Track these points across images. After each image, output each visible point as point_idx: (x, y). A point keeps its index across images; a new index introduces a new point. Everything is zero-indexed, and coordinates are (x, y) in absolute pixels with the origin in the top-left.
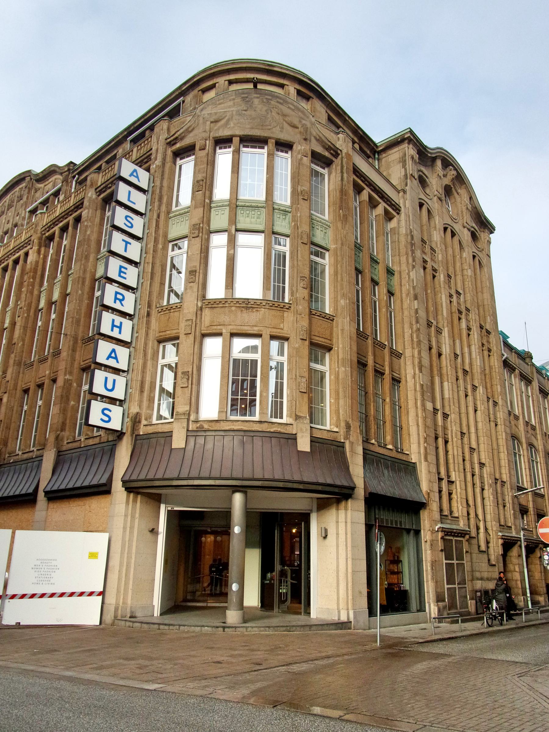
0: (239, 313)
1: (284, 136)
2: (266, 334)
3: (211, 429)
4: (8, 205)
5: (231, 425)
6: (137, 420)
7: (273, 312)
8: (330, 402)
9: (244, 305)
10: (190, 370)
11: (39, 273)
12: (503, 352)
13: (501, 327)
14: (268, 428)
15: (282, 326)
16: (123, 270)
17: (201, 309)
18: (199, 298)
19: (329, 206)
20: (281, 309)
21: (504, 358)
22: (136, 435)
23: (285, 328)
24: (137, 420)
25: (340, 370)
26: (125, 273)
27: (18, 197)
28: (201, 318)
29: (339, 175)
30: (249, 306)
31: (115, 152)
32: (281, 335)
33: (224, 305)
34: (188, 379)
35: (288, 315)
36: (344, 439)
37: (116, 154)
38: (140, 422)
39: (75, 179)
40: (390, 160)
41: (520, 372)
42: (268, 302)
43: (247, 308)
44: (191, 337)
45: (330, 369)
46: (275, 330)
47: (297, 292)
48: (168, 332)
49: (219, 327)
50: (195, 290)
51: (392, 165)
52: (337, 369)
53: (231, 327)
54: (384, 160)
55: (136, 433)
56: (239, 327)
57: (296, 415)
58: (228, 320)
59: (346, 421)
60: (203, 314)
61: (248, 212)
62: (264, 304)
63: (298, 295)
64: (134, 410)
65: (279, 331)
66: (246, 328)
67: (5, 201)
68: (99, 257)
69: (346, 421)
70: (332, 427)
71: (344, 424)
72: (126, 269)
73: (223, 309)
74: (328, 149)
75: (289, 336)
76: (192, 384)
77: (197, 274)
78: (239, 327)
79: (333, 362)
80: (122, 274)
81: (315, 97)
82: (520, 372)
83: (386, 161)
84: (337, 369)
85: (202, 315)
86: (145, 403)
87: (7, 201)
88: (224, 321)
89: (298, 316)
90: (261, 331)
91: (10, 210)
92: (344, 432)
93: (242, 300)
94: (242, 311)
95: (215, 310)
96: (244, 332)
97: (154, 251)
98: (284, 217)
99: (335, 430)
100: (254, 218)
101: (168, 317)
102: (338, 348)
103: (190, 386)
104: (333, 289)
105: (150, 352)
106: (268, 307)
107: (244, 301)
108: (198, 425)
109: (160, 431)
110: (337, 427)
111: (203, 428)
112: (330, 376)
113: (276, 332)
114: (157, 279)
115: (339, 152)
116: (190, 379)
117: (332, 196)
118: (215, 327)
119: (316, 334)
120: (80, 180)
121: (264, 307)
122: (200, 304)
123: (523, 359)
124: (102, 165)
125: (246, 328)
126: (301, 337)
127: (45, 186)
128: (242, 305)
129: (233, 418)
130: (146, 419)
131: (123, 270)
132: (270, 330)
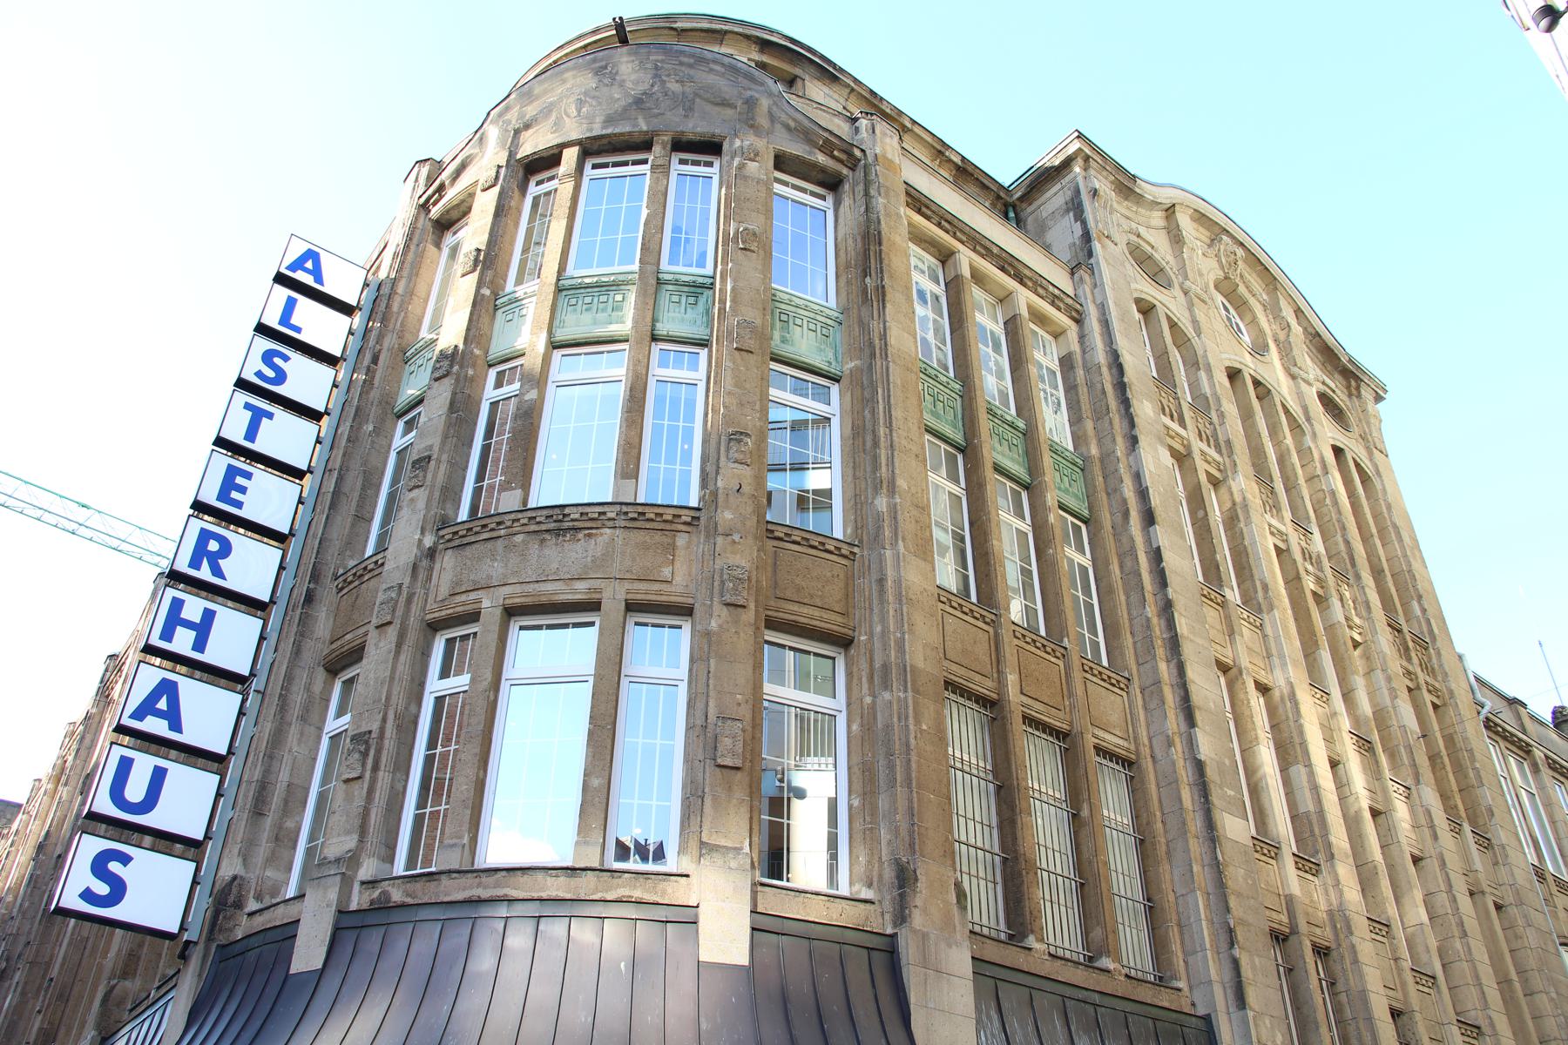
0: (534, 547)
1: (697, 127)
2: (614, 596)
5: (471, 887)
6: (231, 899)
7: (639, 536)
8: (850, 807)
9: (552, 526)
10: (375, 727)
12: (1479, 696)
13: (1475, 665)
14: (596, 890)
15: (666, 572)
16: (239, 480)
17: (431, 554)
18: (428, 527)
19: (837, 277)
20: (668, 527)
21: (1484, 712)
22: (222, 947)
23: (678, 579)
24: (231, 899)
25: (879, 701)
26: (243, 490)
28: (429, 578)
29: (861, 201)
30: (566, 525)
32: (663, 598)
33: (495, 534)
34: (365, 755)
35: (689, 542)
36: (895, 925)
38: (239, 905)
40: (1044, 215)
41: (1547, 757)
42: (625, 509)
43: (558, 532)
44: (392, 632)
45: (849, 705)
46: (643, 586)
47: (717, 473)
48: (348, 637)
49: (473, 596)
50: (421, 504)
51: (1050, 223)
52: (868, 700)
53: (507, 590)
54: (1030, 220)
55: (222, 939)
56: (530, 588)
57: (702, 843)
58: (501, 570)
59: (897, 862)
60: (437, 566)
61: (588, 300)
62: (612, 515)
63: (720, 484)
64: (231, 867)
65: (656, 587)
66: (550, 587)
69: (897, 862)
70: (857, 887)
71: (893, 874)
72: (248, 476)
73: (489, 545)
74: (827, 148)
75: (690, 601)
76: (376, 768)
77: (433, 463)
79: (855, 681)
80: (235, 495)
81: (807, 77)
82: (1547, 757)
83: (1036, 220)
84: (868, 700)
85: (431, 569)
86: (263, 849)
88: (490, 577)
89: (720, 540)
90: (598, 591)
92: (893, 899)
93: (545, 512)
94: (543, 541)
95: (468, 551)
96: (544, 599)
97: (349, 440)
98: (692, 300)
99: (863, 896)
100: (604, 310)
102: (871, 635)
103: (368, 775)
104: (850, 472)
105: (297, 698)
106: (623, 524)
107: (550, 512)
108: (376, 894)
110: (870, 885)
112: (849, 726)
113: (645, 591)
114: (349, 507)
115: (857, 153)
116: (372, 752)
117: (842, 254)
118: (463, 598)
119: (788, 595)
121: (610, 524)
122: (429, 541)
125: (550, 587)
126: (728, 598)
128: (544, 527)
130: (258, 898)
131: (239, 480)
132: (627, 585)
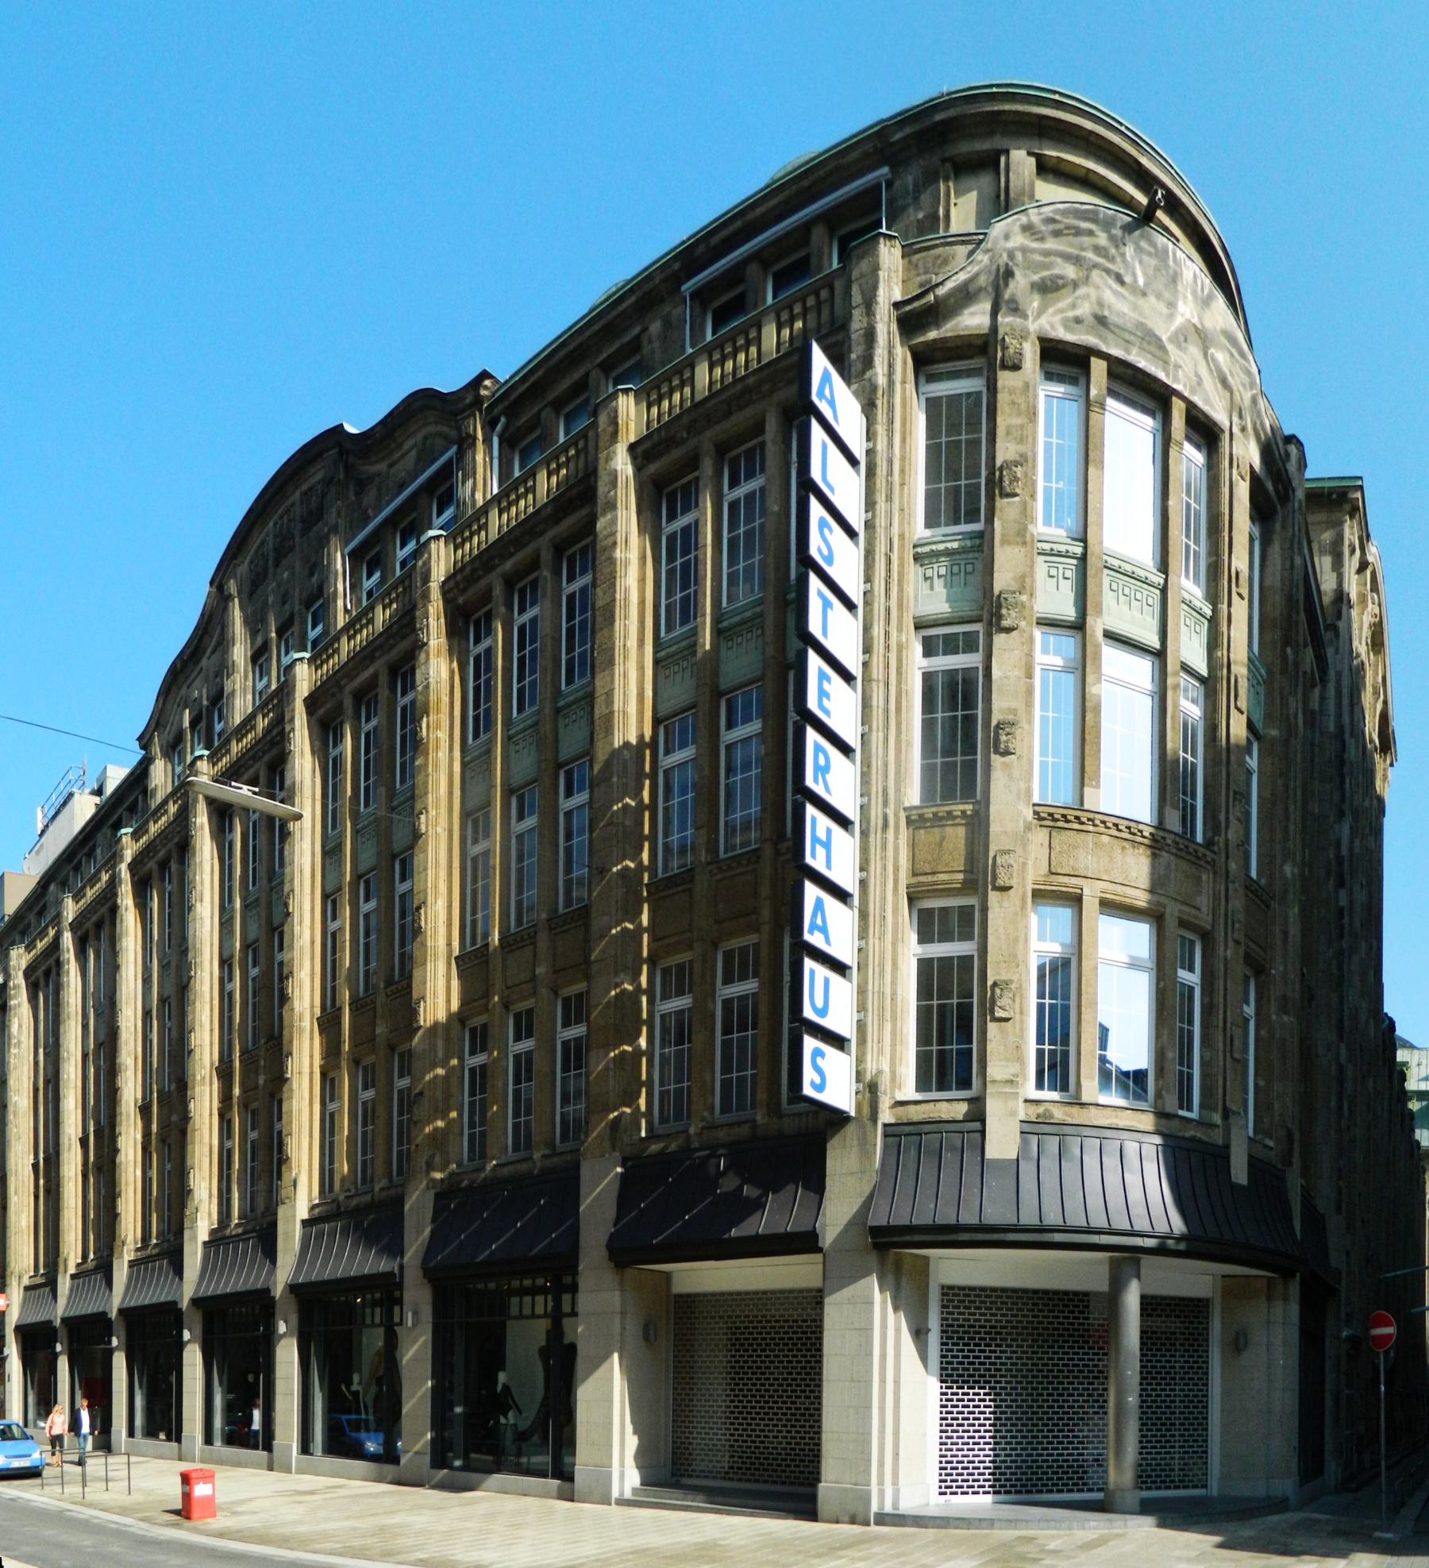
3: (1070, 1121)
4: (275, 549)
7: (1184, 865)
11: (1002, 197)
27: (303, 520)
31: (637, 330)
37: (638, 337)
39: (499, 428)
49: (1074, 881)
67: (263, 543)
68: (395, 803)
78: (1120, 889)
87: (270, 540)
91: (285, 562)
101: (938, 838)
109: (945, 1117)
111: (1052, 1117)
118: (1066, 880)
120: (512, 429)
123: (40, 933)
124: (587, 374)
127: (391, 466)
129: (1103, 1099)
132: (1179, 906)
